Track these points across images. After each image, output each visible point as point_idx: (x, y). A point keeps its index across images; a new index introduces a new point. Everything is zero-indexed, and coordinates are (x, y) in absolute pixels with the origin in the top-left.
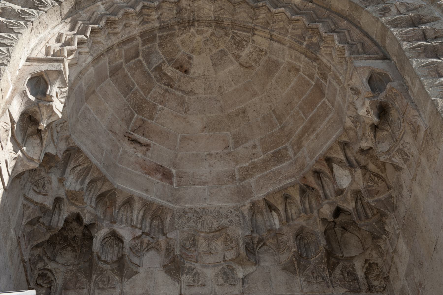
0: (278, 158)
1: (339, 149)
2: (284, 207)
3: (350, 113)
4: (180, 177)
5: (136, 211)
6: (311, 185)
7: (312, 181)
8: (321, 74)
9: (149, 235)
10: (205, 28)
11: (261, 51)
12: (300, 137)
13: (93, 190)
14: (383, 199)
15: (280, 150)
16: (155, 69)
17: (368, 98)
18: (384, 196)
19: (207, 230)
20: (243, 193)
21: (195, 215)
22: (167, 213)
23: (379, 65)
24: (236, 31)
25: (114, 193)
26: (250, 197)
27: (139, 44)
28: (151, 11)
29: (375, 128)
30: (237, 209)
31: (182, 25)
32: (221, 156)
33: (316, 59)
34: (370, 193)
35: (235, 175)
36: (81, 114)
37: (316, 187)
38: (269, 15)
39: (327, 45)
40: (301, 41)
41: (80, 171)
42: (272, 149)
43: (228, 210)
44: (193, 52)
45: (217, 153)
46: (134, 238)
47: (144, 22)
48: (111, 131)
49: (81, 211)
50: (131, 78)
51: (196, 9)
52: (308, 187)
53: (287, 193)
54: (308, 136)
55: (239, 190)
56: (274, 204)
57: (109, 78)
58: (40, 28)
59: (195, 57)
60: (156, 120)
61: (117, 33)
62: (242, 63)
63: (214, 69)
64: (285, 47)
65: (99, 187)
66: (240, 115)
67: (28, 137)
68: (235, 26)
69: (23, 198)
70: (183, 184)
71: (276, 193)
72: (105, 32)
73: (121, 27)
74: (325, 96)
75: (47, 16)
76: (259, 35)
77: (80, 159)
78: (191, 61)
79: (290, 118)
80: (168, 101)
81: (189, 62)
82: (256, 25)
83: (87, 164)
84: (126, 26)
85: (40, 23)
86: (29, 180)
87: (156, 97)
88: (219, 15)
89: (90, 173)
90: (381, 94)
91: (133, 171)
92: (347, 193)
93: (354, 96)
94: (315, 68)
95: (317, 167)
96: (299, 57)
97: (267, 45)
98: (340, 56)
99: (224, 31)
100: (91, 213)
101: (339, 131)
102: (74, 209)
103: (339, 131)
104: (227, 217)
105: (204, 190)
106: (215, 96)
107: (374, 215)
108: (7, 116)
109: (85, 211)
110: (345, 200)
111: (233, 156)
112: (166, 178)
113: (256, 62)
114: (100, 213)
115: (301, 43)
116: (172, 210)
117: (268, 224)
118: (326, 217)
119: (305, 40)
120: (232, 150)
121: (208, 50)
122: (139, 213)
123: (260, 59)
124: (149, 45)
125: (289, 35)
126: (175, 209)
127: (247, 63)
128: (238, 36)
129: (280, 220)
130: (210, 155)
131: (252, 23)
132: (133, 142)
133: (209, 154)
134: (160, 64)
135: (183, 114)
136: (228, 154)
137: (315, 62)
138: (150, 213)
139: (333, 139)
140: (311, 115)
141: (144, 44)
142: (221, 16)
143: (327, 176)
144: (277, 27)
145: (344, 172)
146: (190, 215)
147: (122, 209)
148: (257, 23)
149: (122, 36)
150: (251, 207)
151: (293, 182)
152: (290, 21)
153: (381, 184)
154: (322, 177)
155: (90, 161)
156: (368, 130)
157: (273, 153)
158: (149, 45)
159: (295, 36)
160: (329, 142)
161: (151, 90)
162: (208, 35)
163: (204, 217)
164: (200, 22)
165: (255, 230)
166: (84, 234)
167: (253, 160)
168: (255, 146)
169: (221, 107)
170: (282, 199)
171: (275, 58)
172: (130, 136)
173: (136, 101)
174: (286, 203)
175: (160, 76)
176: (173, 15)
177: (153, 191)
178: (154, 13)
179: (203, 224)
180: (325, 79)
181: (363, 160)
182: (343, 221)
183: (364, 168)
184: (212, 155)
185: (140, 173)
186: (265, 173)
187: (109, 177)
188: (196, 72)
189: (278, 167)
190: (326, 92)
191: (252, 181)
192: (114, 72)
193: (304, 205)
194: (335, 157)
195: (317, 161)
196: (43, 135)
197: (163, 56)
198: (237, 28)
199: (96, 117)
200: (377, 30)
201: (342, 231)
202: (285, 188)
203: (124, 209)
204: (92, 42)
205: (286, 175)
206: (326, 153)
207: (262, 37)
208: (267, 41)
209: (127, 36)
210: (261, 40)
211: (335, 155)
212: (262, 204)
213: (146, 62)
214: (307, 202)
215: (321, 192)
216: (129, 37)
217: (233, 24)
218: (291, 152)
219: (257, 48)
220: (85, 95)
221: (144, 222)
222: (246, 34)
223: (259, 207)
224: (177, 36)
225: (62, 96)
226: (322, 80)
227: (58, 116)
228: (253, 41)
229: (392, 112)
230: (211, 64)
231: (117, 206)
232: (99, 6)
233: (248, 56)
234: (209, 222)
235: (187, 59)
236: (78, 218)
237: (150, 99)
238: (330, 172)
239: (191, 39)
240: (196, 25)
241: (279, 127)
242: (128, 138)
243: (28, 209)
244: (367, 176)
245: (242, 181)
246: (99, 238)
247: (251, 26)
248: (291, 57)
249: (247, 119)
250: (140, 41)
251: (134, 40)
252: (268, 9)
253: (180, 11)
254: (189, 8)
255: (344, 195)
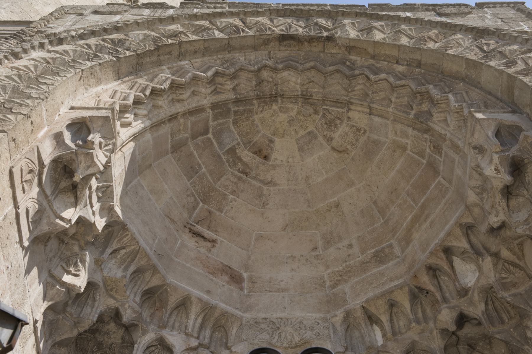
0: (380, 257)
1: (461, 234)
2: (388, 318)
3: (473, 183)
4: (252, 282)
5: (192, 317)
6: (424, 286)
7: (426, 281)
8: (434, 147)
9: (208, 348)
10: (290, 105)
11: (358, 130)
12: (409, 230)
13: (139, 283)
14: (523, 292)
15: (383, 248)
16: (228, 152)
17: (497, 153)
18: (523, 288)
19: (285, 345)
20: (333, 302)
21: (271, 326)
22: (234, 322)
23: (508, 118)
24: (327, 107)
25: (166, 289)
26: (343, 306)
27: (209, 117)
28: (225, 80)
29: (507, 192)
30: (325, 320)
31: (262, 100)
32: (307, 260)
33: (428, 130)
34: (505, 286)
35: (324, 282)
36: (131, 188)
37: (431, 288)
38: (368, 85)
39: (440, 110)
40: (408, 111)
41: (124, 255)
42: (373, 248)
43: (313, 321)
44: (274, 135)
45: (302, 256)
46: (187, 349)
47: (216, 92)
48: (168, 217)
49: (120, 306)
50: (198, 158)
51: (279, 81)
52: (420, 289)
53: (393, 299)
54: (419, 226)
55: (329, 298)
56: (375, 313)
57: (170, 155)
58: (91, 80)
59: (276, 139)
60: (226, 212)
61: (183, 100)
62: (335, 146)
63: (301, 156)
64: (388, 122)
65: (148, 280)
66: (332, 210)
67: (59, 192)
68: (326, 102)
69: (47, 274)
70: (257, 290)
71: (378, 298)
72: (168, 96)
73: (188, 94)
74: (439, 175)
75: (100, 69)
76: (356, 110)
77: (125, 239)
78: (272, 145)
79: (396, 208)
80: (242, 191)
81: (269, 146)
82: (352, 98)
83: (133, 247)
84: (194, 93)
85: (91, 74)
86: (58, 255)
87: (227, 186)
88: (308, 88)
89: (137, 259)
90: (512, 148)
91: (192, 267)
92: (473, 292)
93: (478, 155)
94: (426, 141)
95: (432, 261)
96: (406, 132)
97: (366, 121)
98: (457, 119)
99: (313, 108)
100: (133, 309)
101: (460, 211)
102: (112, 303)
103: (460, 211)
104: (312, 329)
105: (283, 297)
106: (300, 187)
107: (511, 318)
108: (34, 154)
109: (127, 306)
110: (471, 303)
111: (322, 259)
112: (235, 282)
113: (353, 144)
114: (146, 315)
115: (408, 113)
116: (241, 318)
117: (367, 339)
118: (445, 326)
119: (412, 109)
120: (321, 253)
121: (293, 133)
122: (196, 319)
123: (357, 140)
124: (221, 121)
125: (393, 106)
126: (244, 319)
127: (341, 146)
128: (330, 113)
129: (384, 336)
130: (293, 258)
131: (347, 96)
132: (195, 236)
133: (292, 256)
134: (234, 146)
135: (259, 209)
136: (317, 257)
137: (426, 133)
138: (212, 321)
139: (452, 222)
140: (422, 200)
141: (215, 118)
142: (309, 90)
143: (446, 274)
144: (377, 98)
145: (468, 267)
146: (263, 326)
147: (175, 312)
148: (353, 95)
149: (189, 105)
150: (344, 317)
151: (401, 283)
152: (393, 88)
153: (519, 274)
154: (440, 276)
155: (137, 242)
156: (498, 197)
157: (374, 252)
158: (221, 121)
159: (401, 106)
160: (448, 227)
161: (222, 177)
162: (293, 113)
163: (282, 328)
164: (284, 98)
165: (350, 348)
166: (123, 339)
167: (348, 263)
168: (350, 246)
169: (308, 201)
170: (387, 307)
171: (376, 137)
172: (192, 228)
173: (202, 187)
174: (391, 312)
175: (233, 160)
176: (251, 87)
177: (221, 296)
178: (228, 82)
179: (280, 337)
180: (439, 152)
181: (493, 244)
182: (469, 335)
183: (496, 255)
184: (295, 257)
185: (201, 271)
186: (364, 276)
187: (160, 266)
188: (278, 158)
189: (381, 268)
190: (441, 168)
191: (346, 288)
192: (177, 147)
193: (416, 314)
194: (455, 246)
195: (431, 253)
196: (78, 193)
197: (238, 136)
198: (329, 103)
199: (151, 196)
200: (501, 85)
201: (468, 349)
202: (391, 291)
203: (178, 313)
204: (151, 105)
205: (392, 276)
206: (443, 241)
207: (359, 111)
208: (366, 117)
209: (194, 105)
210: (358, 116)
211: (455, 243)
212: (359, 313)
213: (216, 142)
214: (420, 311)
215: (438, 296)
216: (197, 107)
217: (324, 100)
218: (397, 250)
219: (353, 126)
220: (139, 166)
221: (203, 332)
222: (339, 110)
223: (355, 318)
224: (256, 114)
225: (106, 148)
226: (436, 154)
227: (99, 168)
228: (349, 118)
229: (528, 170)
230: (297, 150)
231: (169, 307)
232: (164, 70)
233: (342, 138)
234: (288, 335)
235: (268, 143)
236: (117, 315)
237: (220, 187)
238: (450, 266)
239: (273, 118)
240: (280, 101)
241: (382, 221)
242: (189, 230)
243: (52, 289)
244: (500, 266)
245: (333, 288)
246: (142, 345)
247: (346, 100)
248: (396, 133)
249: (341, 214)
250: (211, 114)
251: (203, 112)
252: (367, 76)
253: (260, 83)
254: (271, 79)
255: (469, 296)
